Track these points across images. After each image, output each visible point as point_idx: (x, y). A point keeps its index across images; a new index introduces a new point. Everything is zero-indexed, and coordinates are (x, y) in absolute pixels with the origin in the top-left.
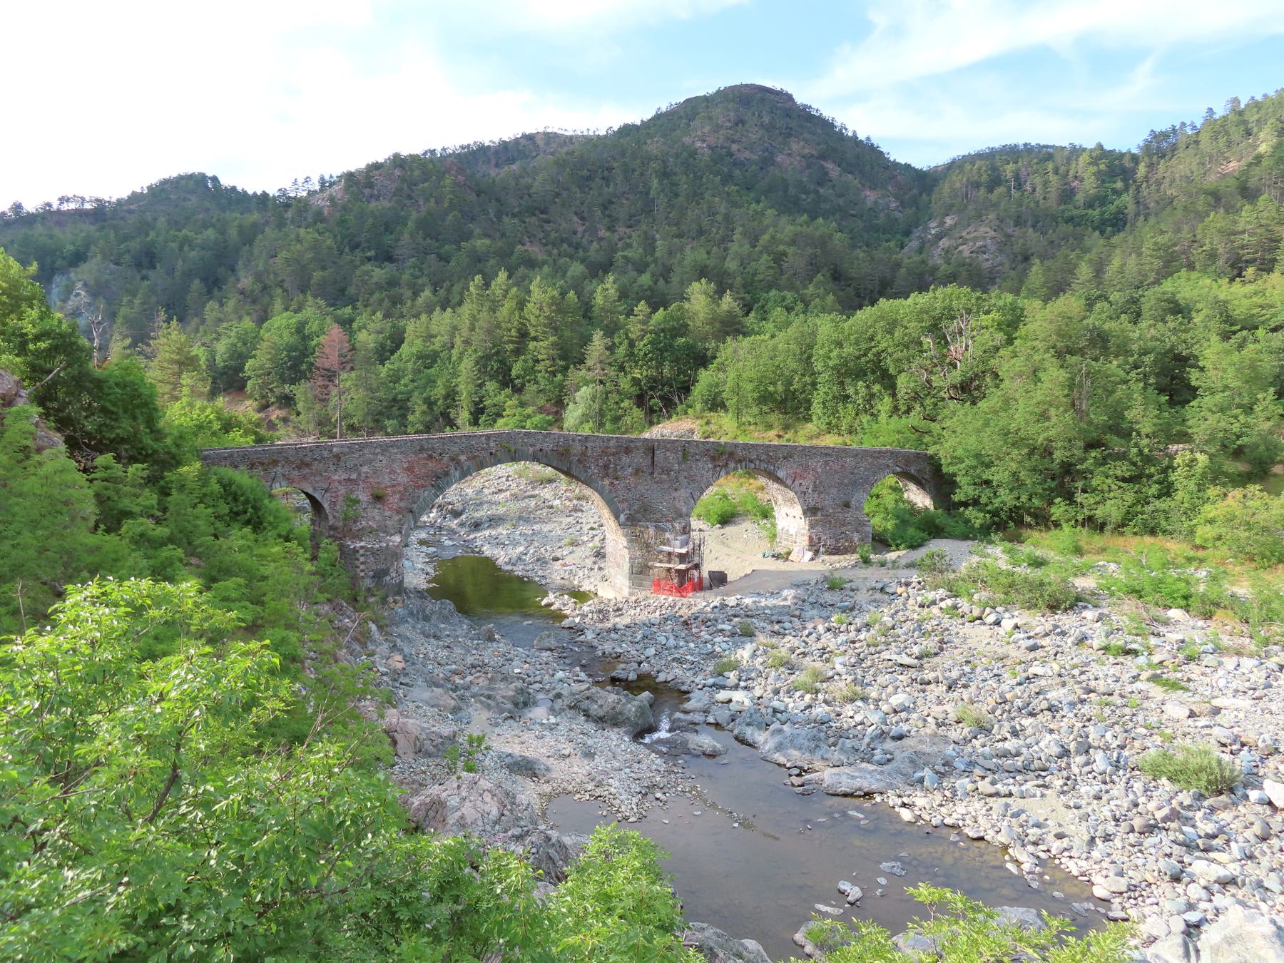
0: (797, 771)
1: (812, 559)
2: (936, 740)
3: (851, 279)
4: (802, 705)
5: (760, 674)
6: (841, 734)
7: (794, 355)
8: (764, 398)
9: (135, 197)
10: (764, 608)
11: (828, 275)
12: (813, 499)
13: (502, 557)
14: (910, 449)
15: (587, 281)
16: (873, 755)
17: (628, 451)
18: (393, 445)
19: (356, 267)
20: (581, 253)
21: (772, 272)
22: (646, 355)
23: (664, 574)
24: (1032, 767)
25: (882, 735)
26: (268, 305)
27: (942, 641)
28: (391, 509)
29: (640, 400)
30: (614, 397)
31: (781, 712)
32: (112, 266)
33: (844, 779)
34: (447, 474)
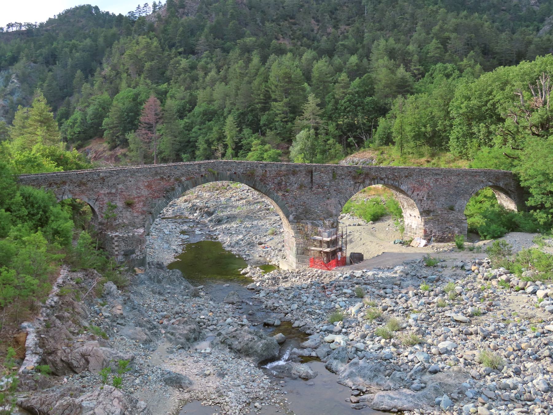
0: (356, 392)
1: (426, 245)
2: (459, 375)
3: (497, 53)
4: (377, 346)
5: (358, 324)
6: (397, 368)
7: (440, 106)
8: (417, 137)
9: (50, 21)
10: (379, 279)
11: (479, 51)
12: (427, 205)
13: (226, 240)
14: (503, 169)
15: (315, 62)
16: (412, 384)
17: (294, 173)
18: (138, 171)
19: (171, 58)
20: (316, 43)
21: (439, 51)
22: (345, 109)
23: (317, 255)
24: (522, 398)
25: (423, 370)
26: (119, 84)
27: (491, 305)
28: (138, 212)
29: (340, 139)
30: (322, 137)
31: (361, 351)
32: (32, 64)
33: (387, 400)
34: (173, 189)
